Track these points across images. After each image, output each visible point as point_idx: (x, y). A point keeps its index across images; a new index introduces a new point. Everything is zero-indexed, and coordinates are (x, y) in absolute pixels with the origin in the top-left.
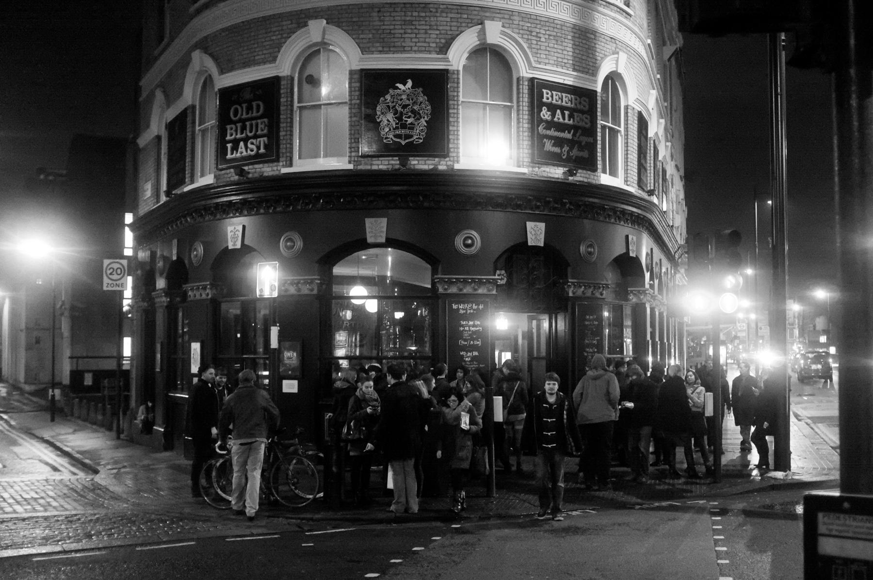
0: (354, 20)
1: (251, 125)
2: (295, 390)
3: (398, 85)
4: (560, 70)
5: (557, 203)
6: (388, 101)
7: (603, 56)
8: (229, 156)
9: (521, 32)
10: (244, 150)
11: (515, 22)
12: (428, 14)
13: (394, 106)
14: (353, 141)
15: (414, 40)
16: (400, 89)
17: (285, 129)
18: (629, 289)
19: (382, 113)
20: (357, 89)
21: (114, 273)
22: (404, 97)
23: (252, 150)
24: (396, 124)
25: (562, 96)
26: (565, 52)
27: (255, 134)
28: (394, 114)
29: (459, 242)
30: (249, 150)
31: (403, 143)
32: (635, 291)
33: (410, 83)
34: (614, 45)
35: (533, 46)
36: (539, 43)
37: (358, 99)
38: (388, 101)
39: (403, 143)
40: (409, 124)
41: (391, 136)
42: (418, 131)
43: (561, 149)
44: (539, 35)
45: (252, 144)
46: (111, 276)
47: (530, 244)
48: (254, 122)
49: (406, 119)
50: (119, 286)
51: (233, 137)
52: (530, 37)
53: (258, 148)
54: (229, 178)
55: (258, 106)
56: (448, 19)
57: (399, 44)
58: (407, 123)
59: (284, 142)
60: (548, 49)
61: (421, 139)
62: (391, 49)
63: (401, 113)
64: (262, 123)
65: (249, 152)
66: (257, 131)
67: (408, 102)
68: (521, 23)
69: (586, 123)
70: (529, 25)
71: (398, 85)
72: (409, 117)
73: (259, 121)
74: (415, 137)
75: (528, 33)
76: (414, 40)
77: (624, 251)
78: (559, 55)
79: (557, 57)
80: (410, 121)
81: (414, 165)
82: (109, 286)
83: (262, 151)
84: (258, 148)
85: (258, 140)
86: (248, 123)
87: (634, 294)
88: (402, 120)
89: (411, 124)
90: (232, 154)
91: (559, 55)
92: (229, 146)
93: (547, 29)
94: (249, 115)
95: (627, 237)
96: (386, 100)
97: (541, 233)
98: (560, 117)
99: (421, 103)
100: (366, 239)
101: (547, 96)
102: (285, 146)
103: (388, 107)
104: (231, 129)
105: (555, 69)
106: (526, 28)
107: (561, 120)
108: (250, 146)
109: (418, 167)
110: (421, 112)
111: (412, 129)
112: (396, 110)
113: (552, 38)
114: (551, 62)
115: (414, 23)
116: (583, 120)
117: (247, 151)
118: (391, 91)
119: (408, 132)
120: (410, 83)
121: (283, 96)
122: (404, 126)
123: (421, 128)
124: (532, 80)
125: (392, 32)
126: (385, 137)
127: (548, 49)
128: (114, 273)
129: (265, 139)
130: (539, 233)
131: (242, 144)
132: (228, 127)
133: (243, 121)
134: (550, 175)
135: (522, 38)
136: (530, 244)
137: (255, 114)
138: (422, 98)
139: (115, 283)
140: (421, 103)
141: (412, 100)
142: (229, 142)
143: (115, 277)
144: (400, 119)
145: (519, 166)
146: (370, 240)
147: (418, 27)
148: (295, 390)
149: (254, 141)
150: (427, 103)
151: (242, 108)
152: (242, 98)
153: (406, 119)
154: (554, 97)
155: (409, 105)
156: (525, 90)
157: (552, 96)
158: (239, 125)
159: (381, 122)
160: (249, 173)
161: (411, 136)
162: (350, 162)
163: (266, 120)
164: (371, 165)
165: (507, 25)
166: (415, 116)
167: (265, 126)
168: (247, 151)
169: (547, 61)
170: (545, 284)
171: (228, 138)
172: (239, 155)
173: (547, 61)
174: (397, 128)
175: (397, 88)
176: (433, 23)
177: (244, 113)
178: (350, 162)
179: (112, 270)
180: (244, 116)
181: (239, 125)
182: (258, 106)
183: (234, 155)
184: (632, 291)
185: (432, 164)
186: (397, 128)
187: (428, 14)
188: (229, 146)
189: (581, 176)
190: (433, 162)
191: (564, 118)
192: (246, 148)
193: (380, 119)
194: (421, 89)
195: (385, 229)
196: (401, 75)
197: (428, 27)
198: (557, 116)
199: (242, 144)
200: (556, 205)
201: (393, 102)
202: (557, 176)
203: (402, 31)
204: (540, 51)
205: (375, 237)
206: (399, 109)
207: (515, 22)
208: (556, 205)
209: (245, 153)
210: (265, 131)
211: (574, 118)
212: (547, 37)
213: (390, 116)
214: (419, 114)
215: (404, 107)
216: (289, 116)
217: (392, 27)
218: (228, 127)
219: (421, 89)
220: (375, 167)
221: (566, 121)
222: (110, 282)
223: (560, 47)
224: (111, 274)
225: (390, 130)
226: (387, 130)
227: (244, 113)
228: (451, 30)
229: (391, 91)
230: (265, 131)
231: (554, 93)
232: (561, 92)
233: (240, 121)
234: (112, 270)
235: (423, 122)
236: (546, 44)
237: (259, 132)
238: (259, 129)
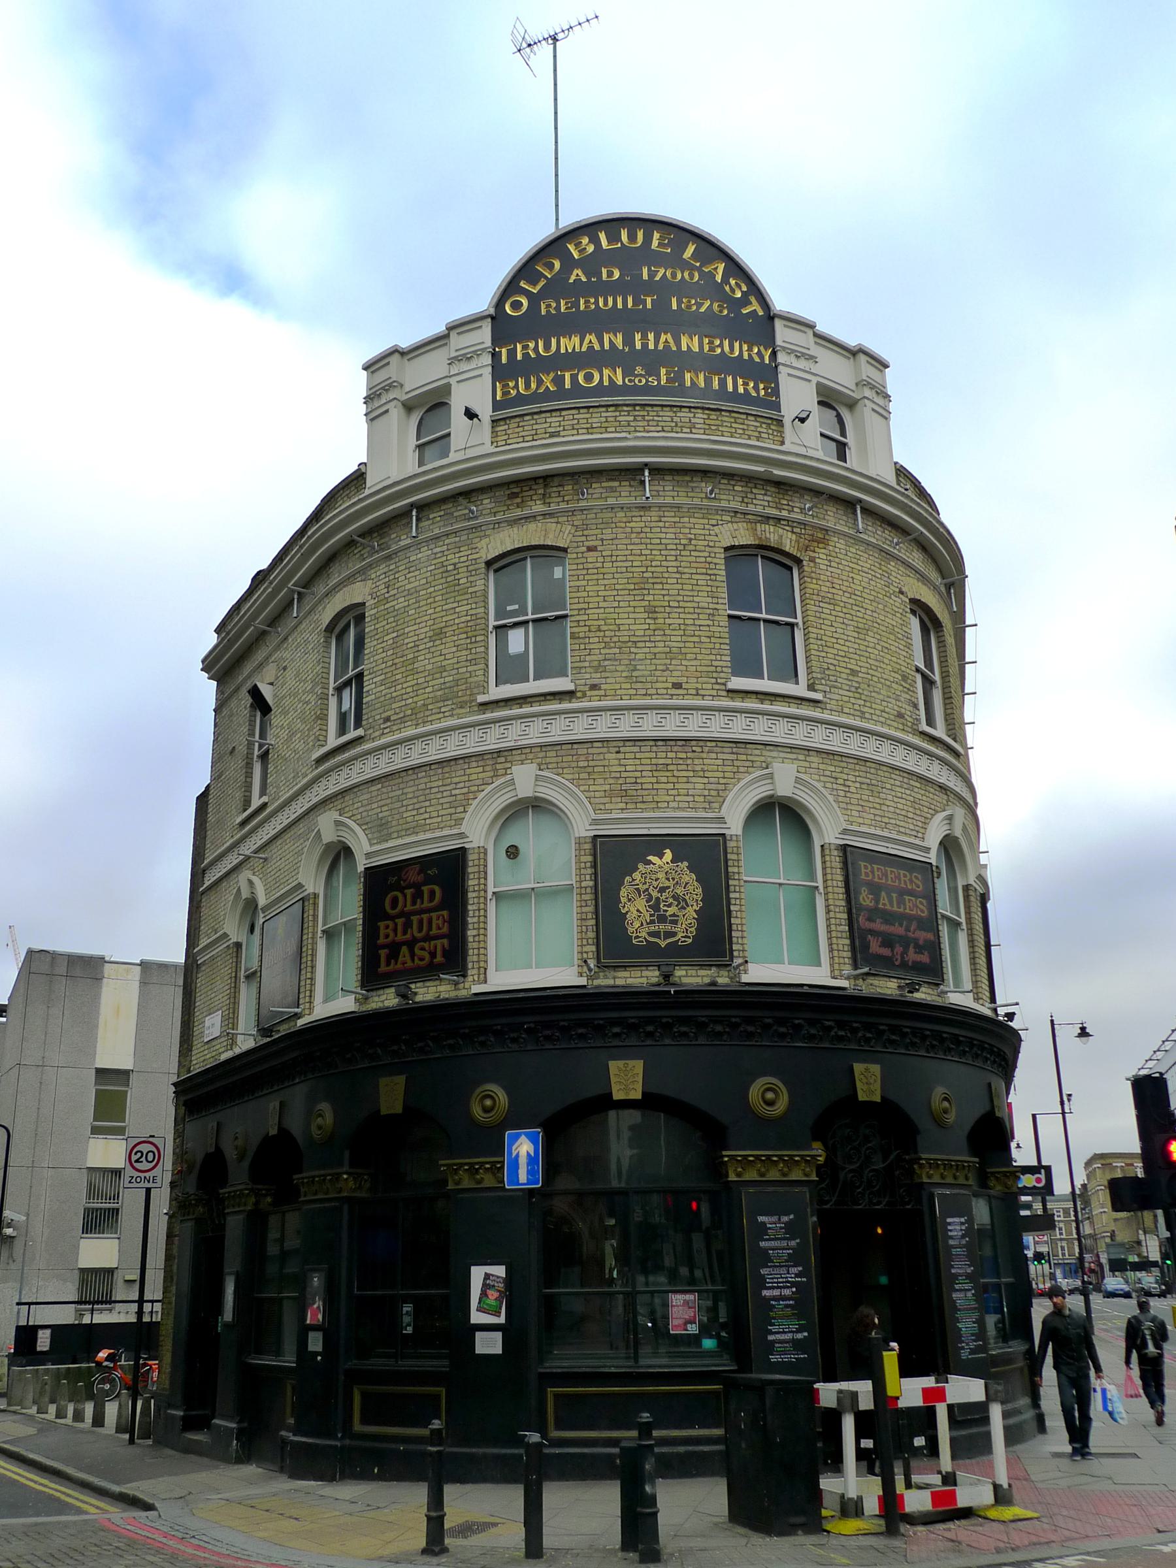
0: (581, 764)
1: (421, 922)
2: (498, 1350)
3: (650, 858)
4: (879, 832)
5: (894, 1034)
6: (637, 882)
7: (933, 812)
8: (383, 968)
9: (822, 778)
10: (408, 959)
11: (813, 765)
12: (689, 755)
13: (647, 890)
14: (585, 942)
15: (671, 792)
16: (654, 864)
17: (476, 926)
18: (988, 1170)
19: (629, 900)
20: (588, 865)
21: (143, 1159)
22: (661, 875)
23: (421, 959)
24: (651, 915)
25: (899, 874)
26: (884, 808)
27: (428, 934)
28: (647, 902)
29: (477, 1111)
30: (416, 958)
31: (663, 944)
32: (999, 1173)
33: (668, 855)
34: (945, 797)
35: (841, 799)
36: (848, 795)
37: (591, 880)
38: (637, 882)
39: (663, 944)
40: (670, 916)
41: (644, 934)
42: (684, 926)
43: (892, 951)
44: (848, 783)
45: (423, 949)
46: (137, 1165)
47: (860, 1099)
48: (425, 916)
49: (665, 908)
50: (149, 1182)
51: (390, 939)
52: (835, 786)
53: (433, 955)
54: (383, 1001)
55: (432, 893)
56: (720, 762)
57: (650, 798)
58: (668, 914)
59: (475, 945)
60: (861, 802)
61: (689, 937)
62: (639, 805)
63: (658, 899)
64: (438, 918)
65: (417, 961)
66: (430, 928)
67: (667, 884)
68: (821, 766)
69: (922, 911)
70: (833, 769)
71: (650, 858)
72: (669, 906)
73: (434, 915)
74: (680, 935)
75: (832, 780)
76: (671, 792)
77: (988, 1108)
78: (877, 812)
79: (875, 815)
80: (671, 911)
81: (680, 977)
82: (133, 1180)
83: (439, 959)
84: (433, 955)
85: (433, 943)
86: (415, 919)
87: (997, 1179)
88: (659, 909)
89: (674, 915)
90: (388, 964)
91: (877, 812)
92: (383, 953)
93: (857, 774)
94: (417, 906)
95: (989, 1085)
96: (633, 880)
97: (875, 1081)
98: (886, 901)
99: (687, 884)
100: (611, 1094)
101: (866, 871)
102: (476, 951)
103: (638, 890)
104: (387, 927)
105: (872, 831)
106: (828, 773)
107: (888, 907)
108: (417, 951)
109: (685, 980)
110: (687, 898)
111: (675, 922)
112: (650, 895)
113: (864, 786)
114: (867, 821)
115: (670, 768)
116: (917, 907)
117: (413, 960)
118: (641, 866)
119: (669, 927)
120: (668, 855)
121: (471, 876)
122: (662, 919)
123: (689, 921)
124: (844, 848)
125: (638, 781)
126: (634, 935)
127: (861, 802)
128: (143, 1159)
129: (445, 941)
130: (872, 1081)
131: (404, 949)
132: (382, 924)
133: (406, 915)
134: (879, 990)
135: (825, 787)
136: (860, 1099)
137: (426, 904)
138: (689, 877)
139: (142, 1175)
140: (687, 884)
141: (673, 879)
142: (383, 947)
143: (144, 1166)
144: (656, 907)
145: (834, 978)
146: (618, 1095)
147: (676, 773)
148: (498, 1350)
149: (426, 945)
150: (695, 883)
151: (405, 896)
152: (405, 881)
153: (665, 908)
154: (876, 873)
155: (669, 887)
156: (835, 860)
157: (873, 872)
158: (400, 921)
159: (627, 912)
160: (416, 994)
161: (674, 934)
162: (581, 975)
163: (445, 913)
164: (614, 978)
165: (803, 770)
166: (679, 903)
167: (445, 921)
168: (413, 960)
169: (861, 821)
170: (884, 1163)
171: (382, 941)
172: (399, 966)
173: (861, 821)
174: (652, 922)
175: (650, 862)
176: (698, 768)
177: (409, 903)
178: (581, 975)
179: (139, 1155)
180: (409, 907)
181: (400, 921)
182: (432, 893)
183: (391, 967)
184: (992, 1173)
185: (707, 976)
186: (652, 922)
187: (689, 755)
188: (383, 953)
189: (923, 995)
190: (709, 972)
191: (891, 904)
192: (413, 955)
193: (626, 909)
194: (686, 864)
195: (640, 1079)
196: (656, 843)
197: (691, 774)
198: (882, 901)
199: (404, 949)
200: (894, 1037)
201: (645, 883)
202: (889, 992)
203: (654, 780)
204: (850, 807)
205: (627, 1090)
206: (655, 894)
207: (813, 765)
208: (894, 1037)
209: (409, 964)
210: (445, 930)
211: (905, 904)
212: (858, 785)
213: (641, 903)
214: (684, 900)
215: (662, 890)
216: (482, 906)
217: (638, 774)
218: (382, 924)
219: (686, 864)
220: (619, 982)
221: (895, 908)
222: (136, 1174)
223: (877, 800)
224: (137, 1161)
225: (642, 925)
226: (637, 924)
227: (409, 903)
228: (724, 778)
229: (641, 866)
230: (445, 930)
231: (875, 866)
232: (884, 865)
233: (402, 914)
234: (139, 1155)
235: (691, 912)
236: (858, 796)
237: (434, 932)
238: (434, 926)
